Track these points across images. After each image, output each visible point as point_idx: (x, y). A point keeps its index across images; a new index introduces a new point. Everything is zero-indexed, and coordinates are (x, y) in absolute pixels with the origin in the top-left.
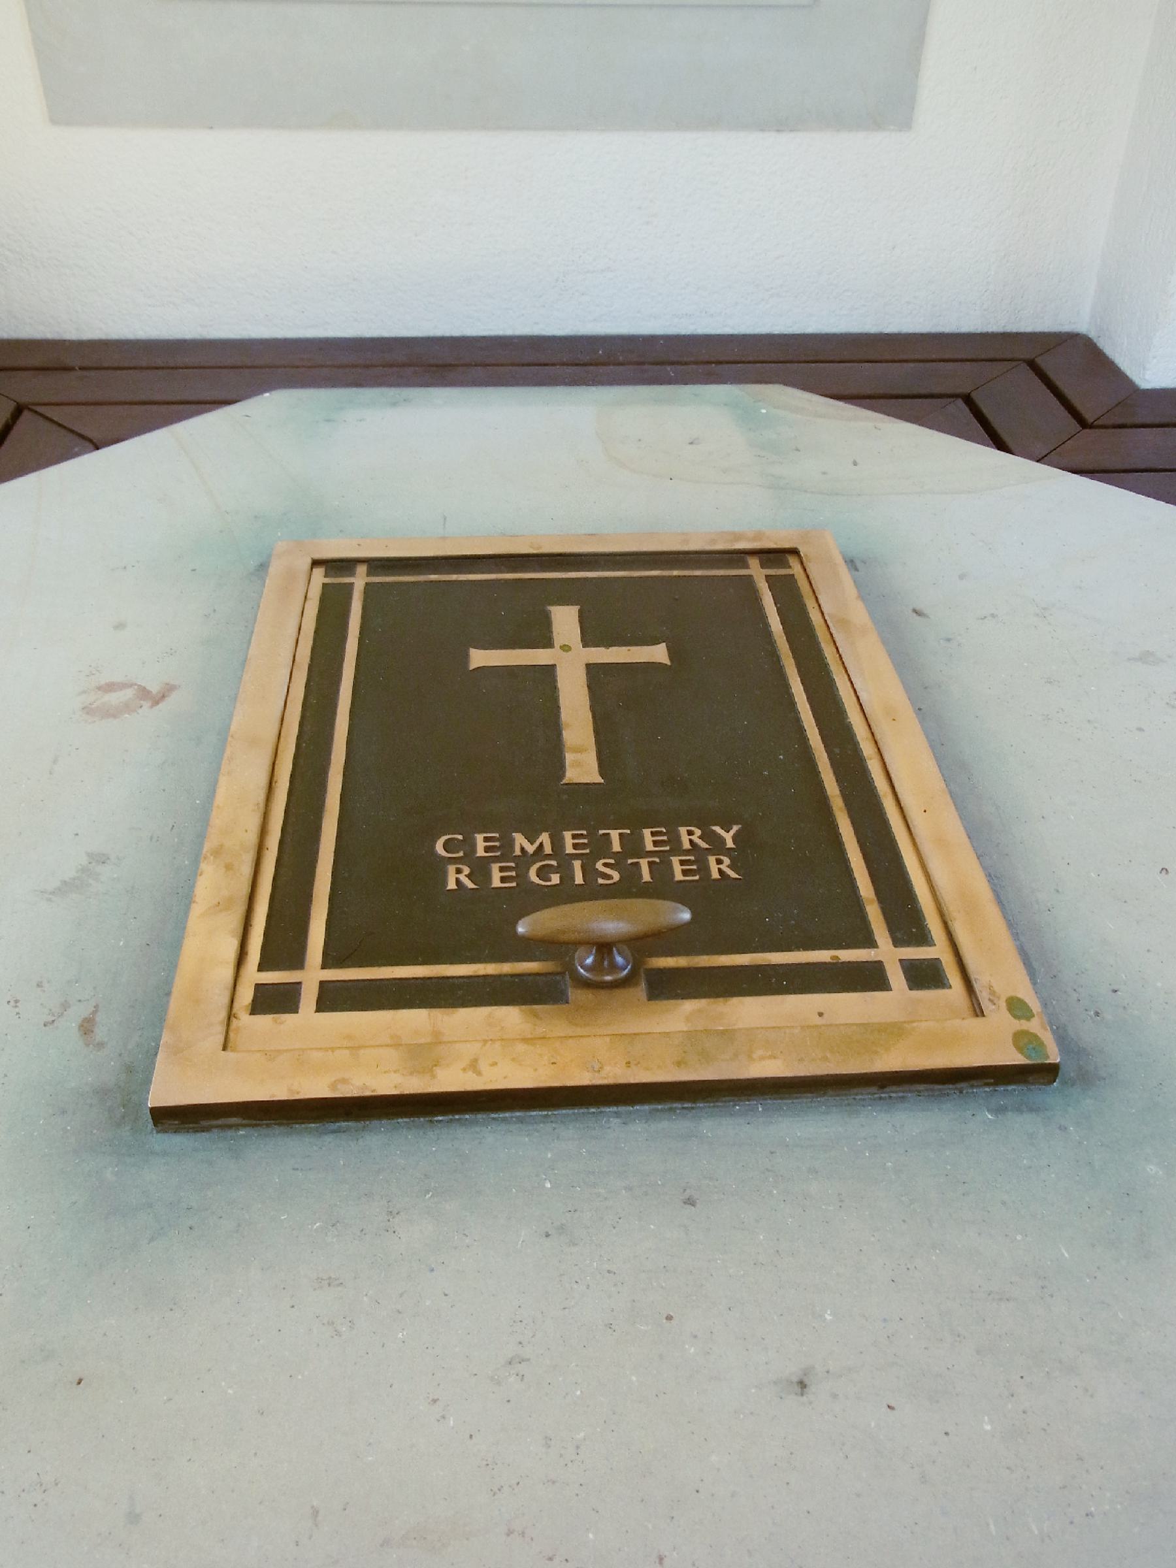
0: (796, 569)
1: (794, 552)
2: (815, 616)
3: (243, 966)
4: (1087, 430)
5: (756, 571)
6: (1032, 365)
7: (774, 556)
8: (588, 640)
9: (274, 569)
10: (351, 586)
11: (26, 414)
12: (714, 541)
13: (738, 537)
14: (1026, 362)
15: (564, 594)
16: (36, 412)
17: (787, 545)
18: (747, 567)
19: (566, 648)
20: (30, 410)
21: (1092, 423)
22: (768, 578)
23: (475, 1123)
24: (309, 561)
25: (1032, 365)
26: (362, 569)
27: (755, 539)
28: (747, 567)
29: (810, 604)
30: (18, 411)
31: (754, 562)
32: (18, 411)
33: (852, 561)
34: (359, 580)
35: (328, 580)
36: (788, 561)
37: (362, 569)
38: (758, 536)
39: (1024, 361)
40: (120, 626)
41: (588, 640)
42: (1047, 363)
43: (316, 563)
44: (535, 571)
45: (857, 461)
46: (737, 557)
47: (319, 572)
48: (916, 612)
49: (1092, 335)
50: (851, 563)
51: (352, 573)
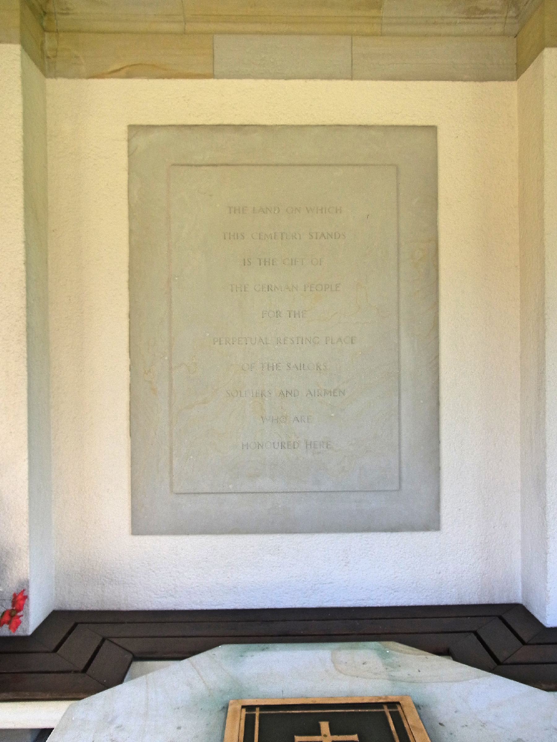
0: (399, 709)
1: (398, 703)
2: (406, 726)
3: (441, 459)
4: (525, 646)
5: (386, 710)
6: (501, 618)
7: (393, 705)
8: (333, 733)
9: (230, 709)
10: (254, 715)
11: (106, 642)
12: (372, 700)
13: (380, 698)
14: (473, 633)
15: (324, 717)
16: (112, 642)
17: (396, 701)
18: (383, 708)
19: (325, 736)
20: (108, 640)
21: (527, 642)
22: (390, 712)
23: (275, 650)
24: (241, 706)
25: (501, 618)
26: (258, 709)
27: (385, 699)
28: (383, 708)
29: (404, 721)
30: (103, 640)
31: (385, 707)
32: (103, 640)
33: (418, 706)
34: (257, 713)
35: (247, 713)
36: (397, 706)
37: (258, 709)
38: (386, 697)
39: (497, 616)
40: (179, 728)
41: (333, 733)
42: (508, 617)
43: (243, 707)
44: (313, 710)
45: (420, 670)
46: (378, 705)
47: (244, 710)
48: (441, 724)
49: (524, 604)
50: (418, 707)
51: (255, 710)
